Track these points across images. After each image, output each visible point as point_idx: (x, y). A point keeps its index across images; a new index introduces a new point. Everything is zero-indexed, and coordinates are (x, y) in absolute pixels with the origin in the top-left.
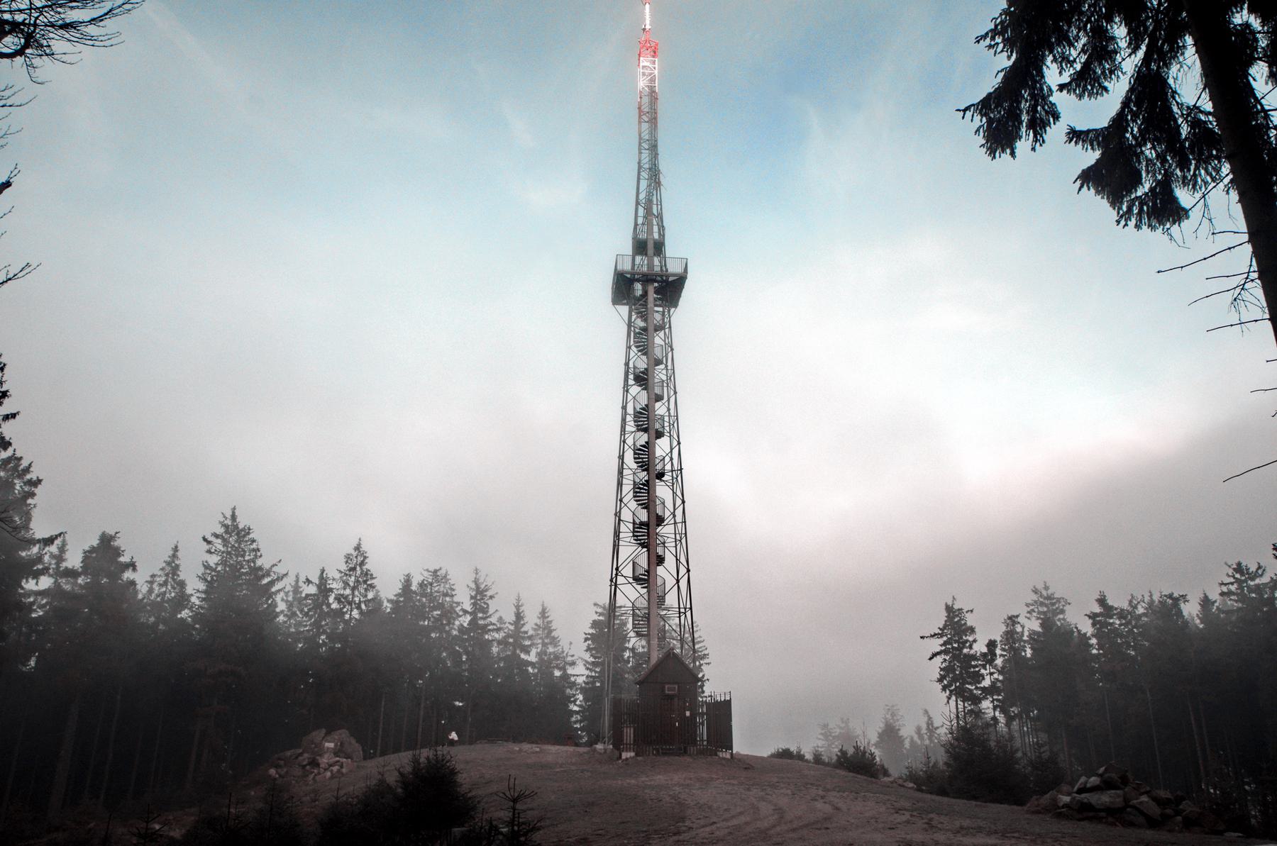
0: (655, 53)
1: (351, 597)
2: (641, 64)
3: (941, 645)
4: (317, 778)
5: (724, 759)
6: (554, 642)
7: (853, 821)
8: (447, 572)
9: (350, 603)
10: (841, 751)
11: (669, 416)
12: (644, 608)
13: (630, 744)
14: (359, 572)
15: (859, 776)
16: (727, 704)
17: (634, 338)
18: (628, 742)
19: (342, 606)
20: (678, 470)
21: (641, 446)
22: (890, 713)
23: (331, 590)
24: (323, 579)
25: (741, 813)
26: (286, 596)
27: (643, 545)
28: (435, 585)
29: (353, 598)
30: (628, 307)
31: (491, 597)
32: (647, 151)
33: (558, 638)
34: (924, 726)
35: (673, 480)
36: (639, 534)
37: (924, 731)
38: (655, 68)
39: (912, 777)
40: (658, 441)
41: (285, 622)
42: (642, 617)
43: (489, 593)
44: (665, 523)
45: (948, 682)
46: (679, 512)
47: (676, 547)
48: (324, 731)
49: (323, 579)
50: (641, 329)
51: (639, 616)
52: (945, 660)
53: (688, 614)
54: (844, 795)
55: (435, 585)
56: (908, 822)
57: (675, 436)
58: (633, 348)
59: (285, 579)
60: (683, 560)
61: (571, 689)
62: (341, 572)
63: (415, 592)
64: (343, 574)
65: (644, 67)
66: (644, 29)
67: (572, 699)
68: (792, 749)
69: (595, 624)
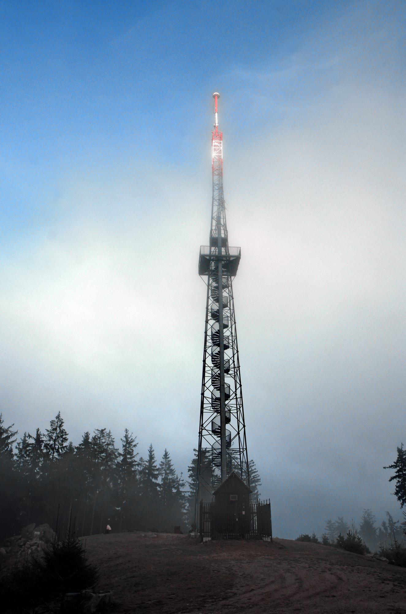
0: (221, 138)
1: (53, 445)
2: (213, 144)
3: (396, 472)
4: (23, 553)
5: (267, 542)
6: (172, 472)
7: (352, 590)
8: (110, 432)
9: (53, 449)
10: (340, 536)
11: (232, 336)
14: (58, 431)
15: (352, 553)
16: (268, 506)
17: (211, 293)
19: (48, 451)
20: (237, 367)
21: (215, 354)
22: (367, 514)
23: (42, 441)
24: (38, 435)
25: (272, 582)
26: (19, 445)
27: (217, 411)
28: (102, 438)
29: (54, 446)
30: (208, 276)
31: (135, 446)
32: (218, 191)
33: (174, 470)
34: (387, 522)
35: (235, 373)
37: (387, 525)
38: (221, 146)
39: (384, 554)
40: (225, 351)
41: (18, 461)
42: (217, 454)
43: (133, 444)
45: (401, 494)
47: (237, 413)
48: (35, 524)
49: (38, 435)
50: (215, 287)
51: (216, 454)
52: (399, 481)
54: (344, 568)
55: (102, 438)
56: (393, 591)
57: (236, 348)
58: (210, 298)
59: (16, 435)
60: (241, 420)
61: (182, 500)
62: (48, 431)
63: (91, 443)
64: (49, 432)
65: (215, 146)
66: (215, 126)
67: (183, 506)
68: (310, 536)
69: (194, 461)
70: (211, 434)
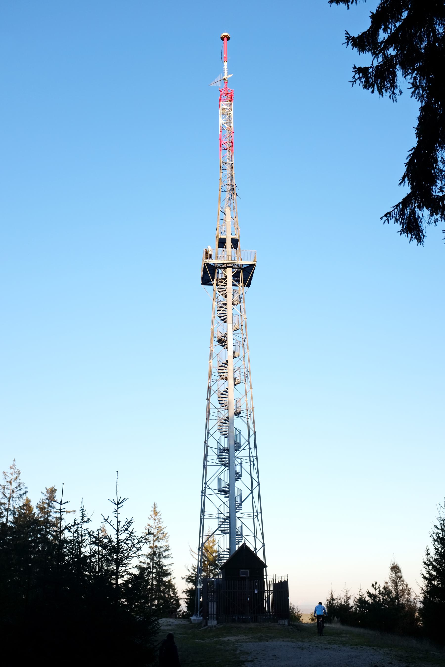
2: (221, 107)
12: (226, 512)
13: (214, 614)
18: (212, 613)
27: (226, 465)
36: (222, 457)
44: (242, 448)
46: (252, 440)
53: (259, 516)
60: (259, 535)
65: (223, 109)
70: (216, 493)
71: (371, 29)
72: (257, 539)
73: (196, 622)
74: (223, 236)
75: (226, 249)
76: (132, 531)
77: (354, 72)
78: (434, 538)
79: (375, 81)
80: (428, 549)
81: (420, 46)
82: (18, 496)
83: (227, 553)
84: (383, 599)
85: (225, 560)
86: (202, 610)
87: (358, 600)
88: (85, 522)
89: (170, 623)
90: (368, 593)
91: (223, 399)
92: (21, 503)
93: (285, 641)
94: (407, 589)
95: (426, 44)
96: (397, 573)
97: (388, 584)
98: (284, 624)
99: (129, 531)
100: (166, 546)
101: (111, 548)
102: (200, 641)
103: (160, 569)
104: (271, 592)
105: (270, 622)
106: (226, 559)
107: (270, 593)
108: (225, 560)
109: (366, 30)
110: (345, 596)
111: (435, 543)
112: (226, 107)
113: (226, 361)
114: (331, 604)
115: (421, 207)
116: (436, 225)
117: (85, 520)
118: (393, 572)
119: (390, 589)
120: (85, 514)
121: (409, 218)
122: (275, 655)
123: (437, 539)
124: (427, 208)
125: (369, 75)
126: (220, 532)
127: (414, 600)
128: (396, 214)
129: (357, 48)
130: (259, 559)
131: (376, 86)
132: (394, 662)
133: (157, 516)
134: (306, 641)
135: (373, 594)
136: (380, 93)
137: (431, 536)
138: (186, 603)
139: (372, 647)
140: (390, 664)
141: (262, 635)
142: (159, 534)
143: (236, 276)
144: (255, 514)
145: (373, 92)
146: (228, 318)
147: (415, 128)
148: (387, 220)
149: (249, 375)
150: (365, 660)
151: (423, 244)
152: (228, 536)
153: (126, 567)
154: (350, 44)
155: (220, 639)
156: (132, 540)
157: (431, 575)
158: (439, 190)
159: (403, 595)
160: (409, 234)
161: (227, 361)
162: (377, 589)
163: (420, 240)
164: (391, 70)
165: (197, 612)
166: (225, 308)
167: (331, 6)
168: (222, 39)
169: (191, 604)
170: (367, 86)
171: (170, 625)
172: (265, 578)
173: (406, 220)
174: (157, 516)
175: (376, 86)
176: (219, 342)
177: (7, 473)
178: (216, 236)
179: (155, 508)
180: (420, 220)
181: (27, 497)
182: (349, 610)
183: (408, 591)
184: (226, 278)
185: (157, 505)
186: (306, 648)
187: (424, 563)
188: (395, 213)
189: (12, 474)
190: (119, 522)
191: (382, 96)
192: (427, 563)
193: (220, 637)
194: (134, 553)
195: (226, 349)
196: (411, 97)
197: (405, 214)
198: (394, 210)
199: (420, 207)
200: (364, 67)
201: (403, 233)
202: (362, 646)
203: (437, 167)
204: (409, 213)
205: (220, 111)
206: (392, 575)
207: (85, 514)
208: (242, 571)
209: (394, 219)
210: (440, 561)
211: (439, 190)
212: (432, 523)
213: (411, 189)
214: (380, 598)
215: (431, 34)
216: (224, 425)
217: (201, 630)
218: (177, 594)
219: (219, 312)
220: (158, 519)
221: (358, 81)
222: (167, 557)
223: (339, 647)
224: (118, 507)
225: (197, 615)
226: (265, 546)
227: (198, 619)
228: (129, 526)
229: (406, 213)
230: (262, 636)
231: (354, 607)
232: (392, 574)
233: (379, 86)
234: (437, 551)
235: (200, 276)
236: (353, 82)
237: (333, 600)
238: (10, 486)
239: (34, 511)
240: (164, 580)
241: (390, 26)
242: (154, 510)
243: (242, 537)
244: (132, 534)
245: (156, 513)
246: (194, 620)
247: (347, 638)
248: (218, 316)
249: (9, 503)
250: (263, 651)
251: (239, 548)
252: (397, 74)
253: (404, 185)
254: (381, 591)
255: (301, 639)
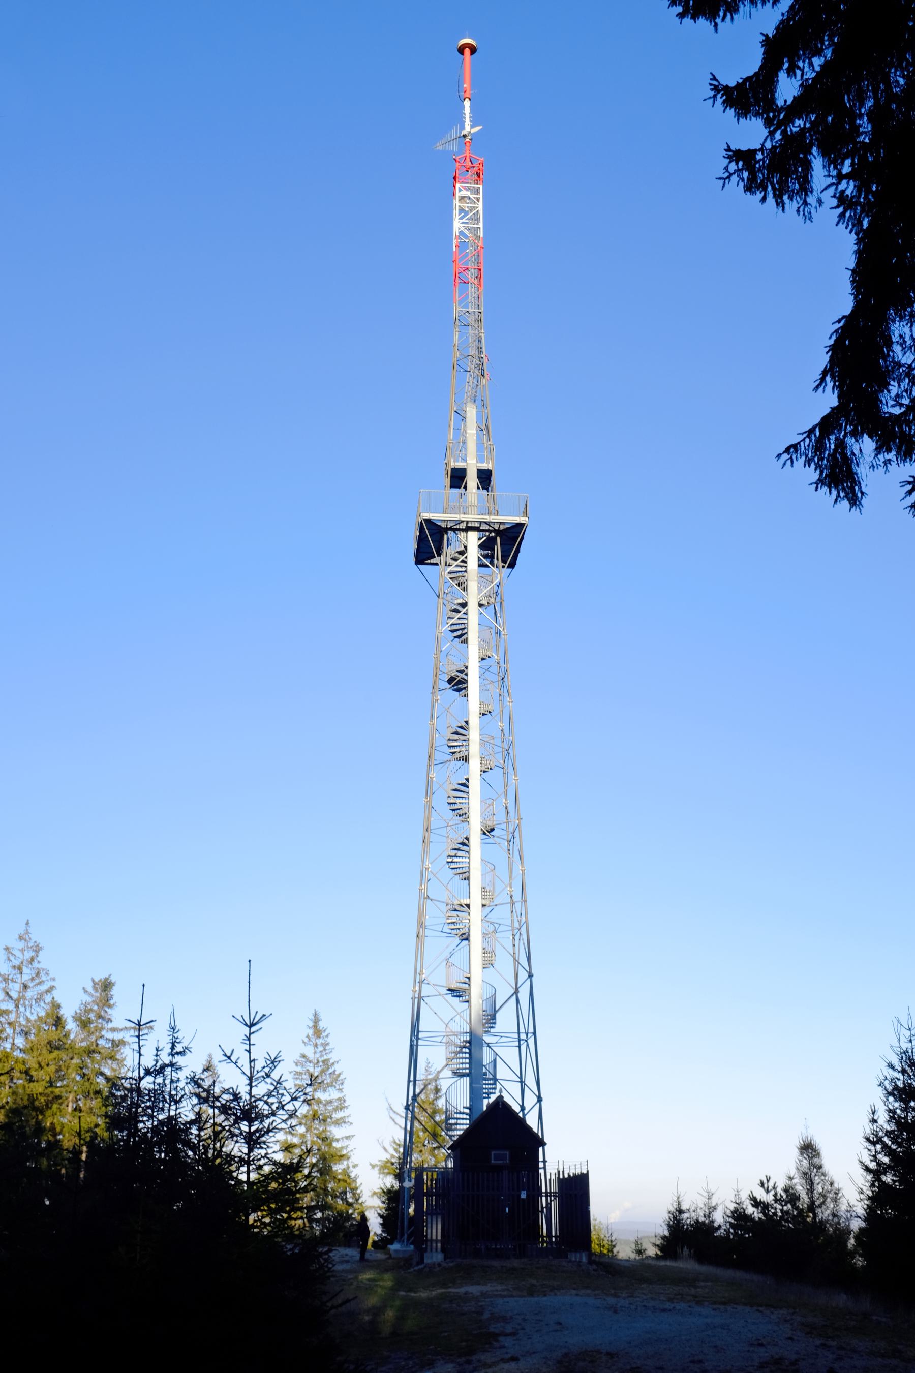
0: (479, 176)
2: (458, 194)
18: (434, 1237)
53: (531, 1041)
60: (530, 1080)
63: (82, 1161)
65: (462, 198)
71: (763, 72)
72: (526, 1089)
73: (401, 1256)
74: (460, 464)
75: (466, 490)
76: (279, 1078)
77: (728, 158)
78: (886, 1089)
79: (768, 179)
80: (873, 1109)
81: (860, 111)
82: (35, 997)
83: (464, 1116)
84: (782, 1211)
85: (460, 1130)
86: (413, 1230)
87: (732, 1212)
88: (177, 1053)
89: (346, 1258)
90: (751, 1199)
91: (458, 801)
92: (41, 1011)
93: (581, 1296)
94: (831, 1190)
95: (871, 106)
96: (812, 1158)
97: (795, 1181)
98: (580, 1262)
99: (274, 1080)
100: (339, 1099)
101: (237, 1113)
102: (409, 1294)
103: (326, 1148)
104: (554, 1196)
105: (550, 1257)
106: (461, 1127)
107: (552, 1198)
108: (460, 1130)
109: (751, 74)
110: (705, 1205)
111: (888, 1100)
112: (468, 193)
113: (465, 722)
114: (676, 1220)
115: (858, 434)
116: (887, 471)
117: (178, 1051)
118: (805, 1156)
119: (798, 1190)
120: (177, 1038)
121: (833, 456)
122: (560, 1324)
123: (893, 1089)
124: (871, 437)
125: (757, 166)
126: (450, 1074)
127: (846, 1213)
128: (807, 448)
129: (733, 110)
130: (529, 1129)
131: (770, 188)
132: (798, 1336)
133: (320, 1037)
134: (624, 1295)
135: (762, 1200)
136: (778, 204)
137: (880, 1085)
138: (381, 1216)
139: (755, 1308)
140: (790, 1341)
141: (534, 1282)
142: (325, 1074)
143: (486, 546)
144: (523, 1036)
145: (764, 200)
146: (469, 633)
147: (851, 270)
148: (789, 460)
149: (511, 751)
150: (740, 1332)
151: (860, 510)
152: (466, 1080)
153: (268, 1149)
154: (719, 100)
155: (450, 1290)
156: (280, 1096)
157: (879, 1164)
158: (894, 403)
159: (823, 1203)
160: (833, 490)
161: (467, 722)
162: (771, 1190)
163: (854, 501)
164: (801, 156)
165: (402, 1235)
166: (464, 613)
167: (681, 23)
168: (461, 50)
169: (390, 1220)
170: (753, 187)
171: (347, 1262)
172: (541, 1168)
173: (828, 461)
174: (320, 1037)
175: (770, 188)
176: (450, 684)
177: (13, 948)
178: (446, 464)
179: (316, 1021)
180: (855, 461)
181: (53, 998)
182: (715, 1232)
183: (834, 1196)
184: (466, 551)
185: (322, 1016)
186: (623, 1309)
187: (865, 1140)
188: (806, 445)
189: (22, 951)
190: (254, 1060)
191: (783, 210)
192: (871, 1139)
193: (450, 1287)
194: (284, 1121)
195: (465, 696)
196: (837, 225)
197: (825, 449)
198: (804, 440)
199: (856, 434)
200: (747, 149)
201: (821, 487)
202: (735, 1306)
203: (891, 354)
204: (833, 447)
205: (456, 202)
206: (801, 1163)
207: (177, 1038)
208: (494, 1160)
209: (803, 458)
210: (897, 1134)
211: (894, 403)
212: (884, 1059)
213: (839, 397)
214: (776, 1209)
215: (881, 85)
216: (459, 853)
217: (409, 1273)
218: (360, 1197)
219: (451, 621)
220: (322, 1044)
221: (735, 178)
222: (341, 1123)
223: (690, 1307)
224: (251, 1032)
225: (403, 1241)
226: (542, 1103)
227: (404, 1249)
228: (273, 1068)
229: (828, 446)
230: (533, 1285)
231: (724, 1227)
232: (802, 1161)
233: (776, 188)
234: (891, 1115)
235: (413, 546)
236: (725, 179)
237: (681, 1212)
238: (19, 976)
239: (68, 1027)
240: (334, 1169)
241: (801, 64)
242: (314, 1026)
243: (495, 1084)
244: (278, 1085)
245: (318, 1032)
246: (396, 1251)
247: (707, 1290)
248: (449, 629)
249: (17, 1011)
250: (536, 1314)
251: (489, 1106)
252: (813, 165)
253: (824, 391)
254: (779, 1195)
255: (613, 1292)
